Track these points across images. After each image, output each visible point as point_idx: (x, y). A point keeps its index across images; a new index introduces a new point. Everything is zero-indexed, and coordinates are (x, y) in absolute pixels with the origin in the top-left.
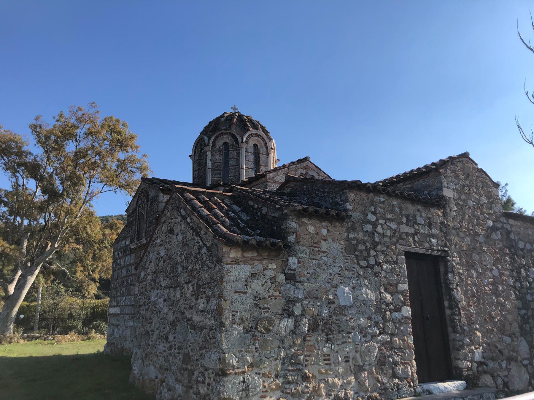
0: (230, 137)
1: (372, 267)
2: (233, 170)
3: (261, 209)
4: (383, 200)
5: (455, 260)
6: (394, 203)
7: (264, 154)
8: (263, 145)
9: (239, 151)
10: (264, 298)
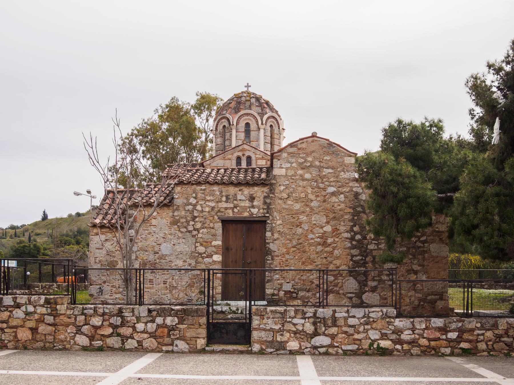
8: (277, 127)
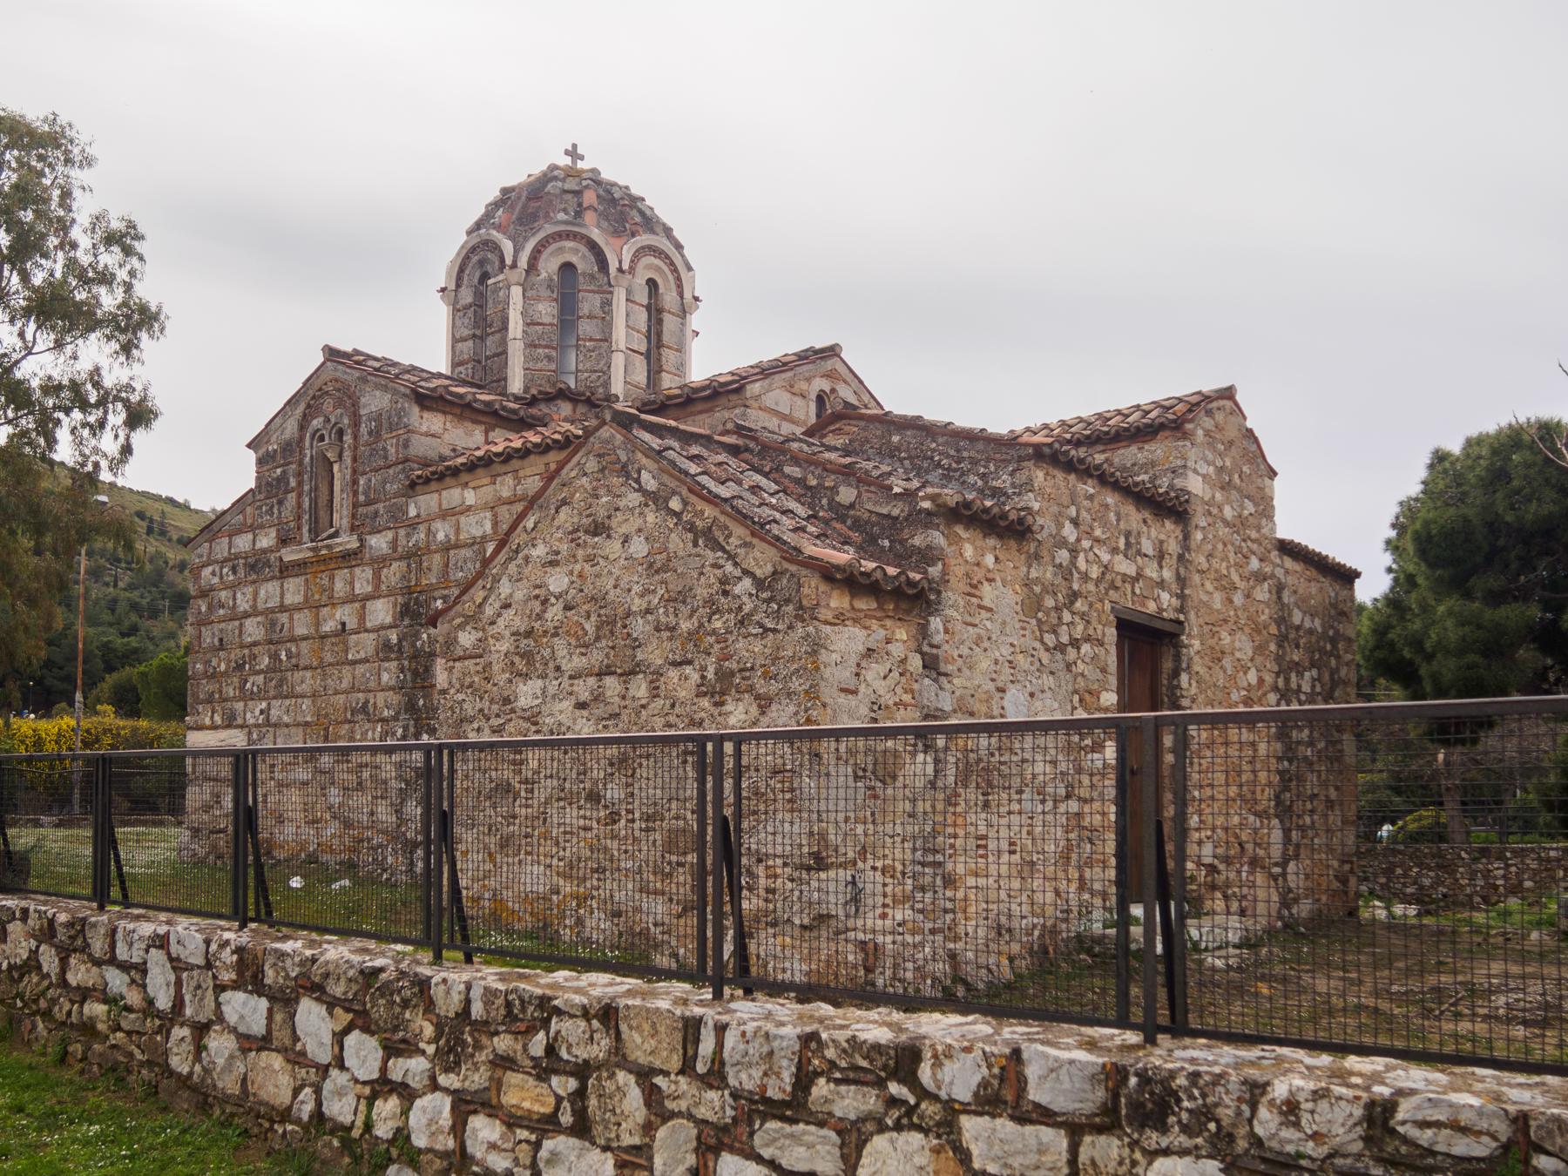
0: (583, 249)
1: (1060, 648)
2: (589, 351)
3: (834, 490)
4: (1091, 491)
5: (1193, 644)
6: (1110, 500)
7: (673, 314)
8: (673, 287)
9: (609, 296)
10: (887, 707)
